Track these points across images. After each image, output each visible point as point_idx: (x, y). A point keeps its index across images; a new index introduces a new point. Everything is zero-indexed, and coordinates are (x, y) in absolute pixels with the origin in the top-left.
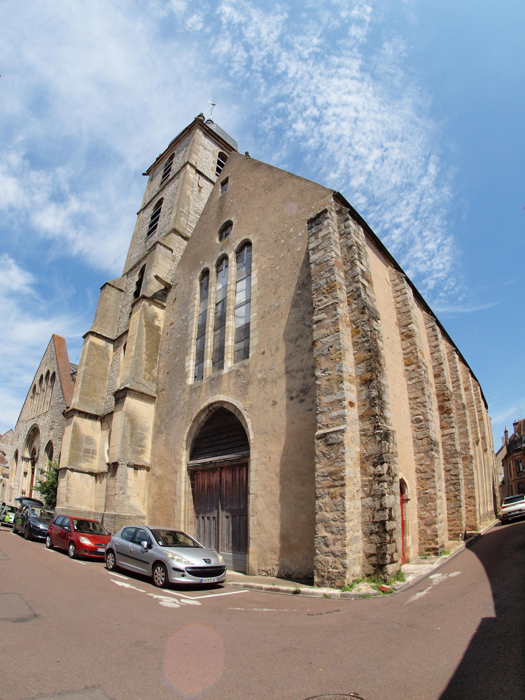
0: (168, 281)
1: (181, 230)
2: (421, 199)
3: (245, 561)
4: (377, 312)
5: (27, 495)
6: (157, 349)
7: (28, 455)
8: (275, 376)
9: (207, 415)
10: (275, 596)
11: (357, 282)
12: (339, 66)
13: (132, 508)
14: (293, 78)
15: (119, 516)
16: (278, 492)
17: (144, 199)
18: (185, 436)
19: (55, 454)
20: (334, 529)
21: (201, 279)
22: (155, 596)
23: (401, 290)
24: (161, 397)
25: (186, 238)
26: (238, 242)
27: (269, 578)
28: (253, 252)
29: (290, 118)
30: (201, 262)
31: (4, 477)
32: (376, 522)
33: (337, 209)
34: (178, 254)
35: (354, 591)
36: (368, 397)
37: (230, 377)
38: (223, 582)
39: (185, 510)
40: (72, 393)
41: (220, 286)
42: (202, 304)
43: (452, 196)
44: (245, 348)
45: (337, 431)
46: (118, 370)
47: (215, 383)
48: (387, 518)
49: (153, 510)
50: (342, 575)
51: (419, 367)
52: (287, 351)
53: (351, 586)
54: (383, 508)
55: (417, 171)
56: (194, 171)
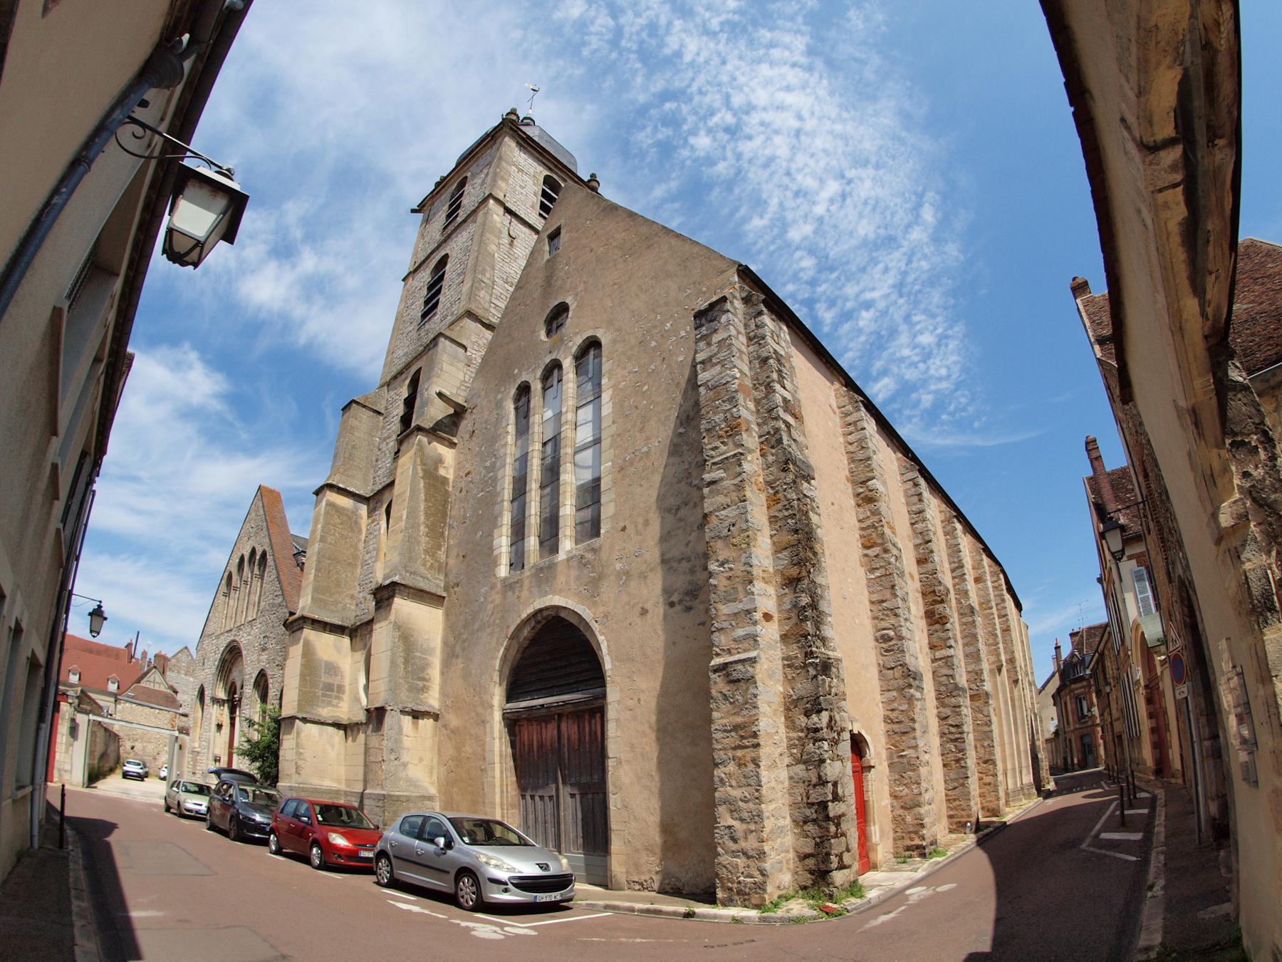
0: (460, 401)
1: (480, 312)
2: (909, 262)
3: (606, 867)
4: (809, 466)
5: (223, 764)
6: (445, 515)
7: (222, 694)
8: (644, 567)
10: (655, 920)
11: (776, 419)
12: (772, 45)
13: (412, 783)
14: (692, 64)
15: (390, 796)
16: (654, 755)
17: (415, 254)
18: (497, 663)
19: (273, 692)
20: (745, 815)
21: (517, 399)
22: (464, 924)
23: (855, 423)
24: (454, 597)
25: (489, 327)
26: (579, 340)
27: (646, 893)
28: (604, 359)
29: (685, 128)
31: (181, 732)
32: (813, 804)
33: (744, 295)
34: (477, 355)
35: (780, 913)
36: (795, 606)
37: (569, 567)
38: (571, 900)
39: (502, 785)
40: (298, 588)
41: (549, 414)
42: (519, 442)
43: (961, 258)
44: (592, 520)
45: (744, 660)
46: (377, 550)
47: (545, 575)
48: (830, 797)
49: (448, 785)
50: (761, 887)
51: (886, 551)
52: (662, 528)
53: (776, 905)
54: (822, 782)
55: (902, 217)
56: (501, 210)
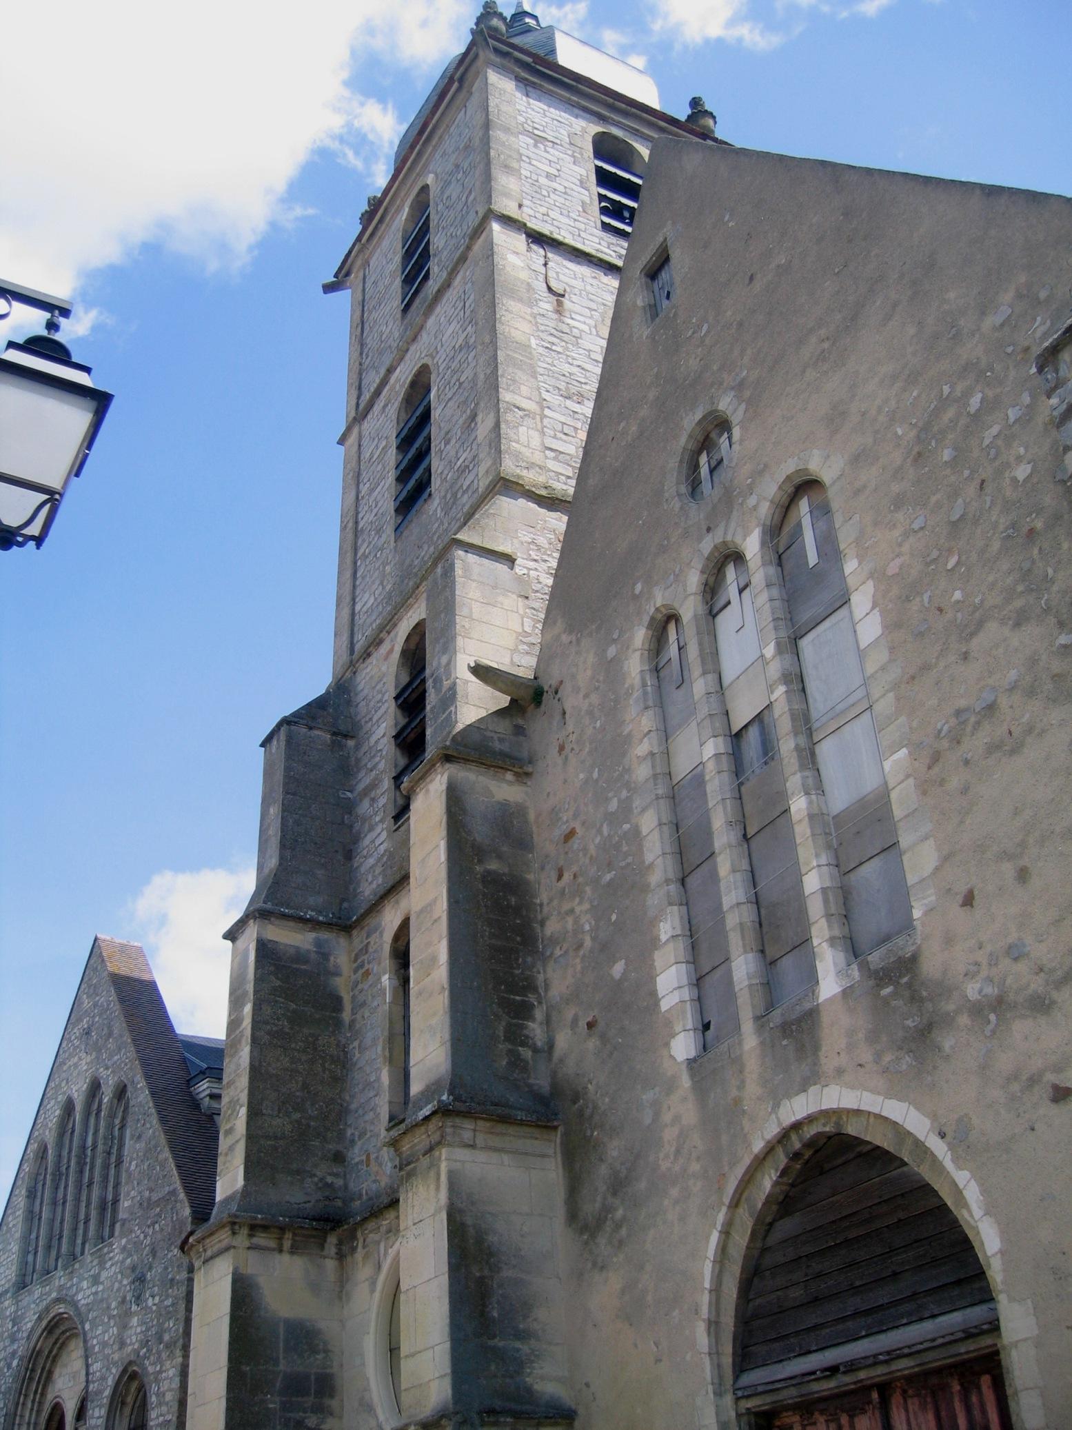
9: (784, 1173)
18: (708, 1269)
25: (550, 502)
26: (770, 489)
30: (638, 587)
56: (520, 240)
